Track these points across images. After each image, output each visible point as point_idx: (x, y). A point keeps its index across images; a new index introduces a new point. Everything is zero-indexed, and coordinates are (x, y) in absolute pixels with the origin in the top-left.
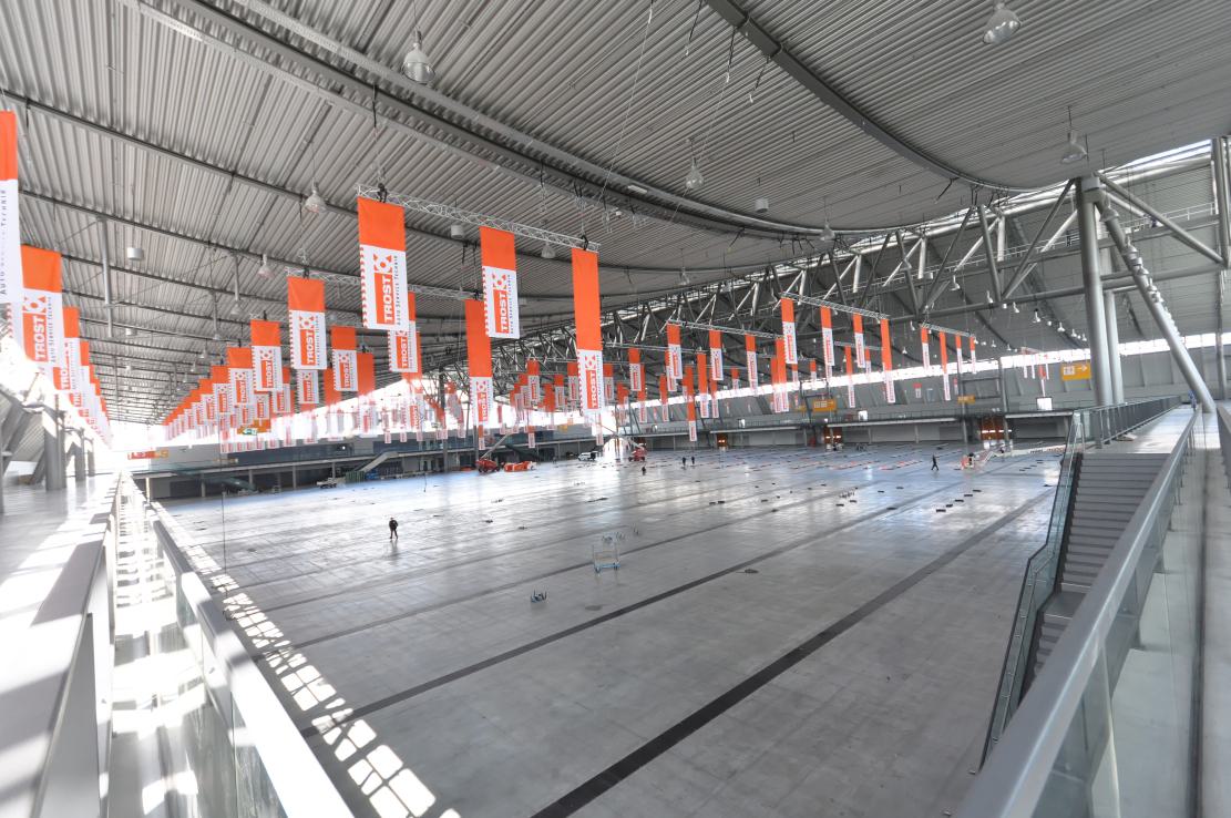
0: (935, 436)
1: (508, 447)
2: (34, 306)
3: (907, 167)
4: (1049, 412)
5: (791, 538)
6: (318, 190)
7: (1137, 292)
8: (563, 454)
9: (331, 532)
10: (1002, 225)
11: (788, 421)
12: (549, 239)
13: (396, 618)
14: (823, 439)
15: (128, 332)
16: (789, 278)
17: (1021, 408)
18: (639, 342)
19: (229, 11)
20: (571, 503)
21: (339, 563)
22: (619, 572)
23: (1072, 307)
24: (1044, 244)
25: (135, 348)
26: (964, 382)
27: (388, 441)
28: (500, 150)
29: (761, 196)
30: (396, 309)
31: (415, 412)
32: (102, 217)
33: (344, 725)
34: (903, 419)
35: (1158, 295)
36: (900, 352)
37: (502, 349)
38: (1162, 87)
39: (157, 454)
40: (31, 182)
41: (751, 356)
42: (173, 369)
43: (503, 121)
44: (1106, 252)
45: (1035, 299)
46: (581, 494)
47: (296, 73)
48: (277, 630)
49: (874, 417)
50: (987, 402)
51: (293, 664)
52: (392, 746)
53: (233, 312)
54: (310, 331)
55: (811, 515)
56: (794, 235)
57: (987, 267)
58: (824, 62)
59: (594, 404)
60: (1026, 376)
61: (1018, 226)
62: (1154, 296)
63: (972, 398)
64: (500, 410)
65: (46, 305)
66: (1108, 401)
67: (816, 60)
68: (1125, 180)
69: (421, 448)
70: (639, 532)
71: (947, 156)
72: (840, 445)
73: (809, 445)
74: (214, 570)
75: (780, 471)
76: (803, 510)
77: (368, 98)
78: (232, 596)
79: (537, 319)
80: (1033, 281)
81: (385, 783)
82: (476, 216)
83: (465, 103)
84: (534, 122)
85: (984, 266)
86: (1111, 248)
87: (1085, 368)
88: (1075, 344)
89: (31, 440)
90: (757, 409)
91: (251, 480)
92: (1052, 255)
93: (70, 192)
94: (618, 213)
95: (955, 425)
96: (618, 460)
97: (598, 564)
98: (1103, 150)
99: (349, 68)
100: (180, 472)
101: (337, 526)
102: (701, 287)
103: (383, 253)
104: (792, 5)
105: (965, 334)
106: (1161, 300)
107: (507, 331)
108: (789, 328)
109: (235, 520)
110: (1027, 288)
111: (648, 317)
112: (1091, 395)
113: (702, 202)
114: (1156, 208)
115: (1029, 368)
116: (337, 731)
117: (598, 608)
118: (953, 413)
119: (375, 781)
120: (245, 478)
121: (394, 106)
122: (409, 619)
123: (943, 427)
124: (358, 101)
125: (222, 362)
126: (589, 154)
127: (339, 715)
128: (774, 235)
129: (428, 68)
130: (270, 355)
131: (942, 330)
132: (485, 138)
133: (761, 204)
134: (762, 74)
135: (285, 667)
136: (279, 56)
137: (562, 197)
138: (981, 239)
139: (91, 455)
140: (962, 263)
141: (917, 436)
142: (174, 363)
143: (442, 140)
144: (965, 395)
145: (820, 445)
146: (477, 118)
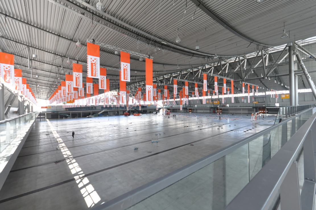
0: (247, 112)
1: (135, 109)
2: (7, 68)
3: (238, 39)
4: (278, 107)
5: (207, 136)
6: (79, 41)
7: (304, 75)
8: (149, 112)
9: (88, 129)
10: (268, 56)
11: (208, 106)
12: (141, 56)
13: (100, 152)
14: (217, 111)
15: (37, 76)
16: (209, 68)
17: (271, 106)
18: (169, 84)
19: (73, 2)
20: (151, 125)
21: (88, 137)
22: (158, 143)
23: (286, 79)
24: (279, 61)
25: (41, 81)
26: (255, 98)
27: (104, 107)
28: (127, 31)
29: (197, 45)
30: (96, 72)
31: (107, 100)
32: (28, 46)
33: (82, 178)
34: (238, 107)
35: (310, 76)
36: (238, 89)
37: (134, 84)
38: (312, 17)
39: (48, 107)
40: (10, 37)
41: (196, 89)
42: (50, 86)
43: (127, 23)
44: (296, 64)
45: (275, 76)
46: (152, 123)
47: (75, 10)
48: (70, 153)
49: (230, 106)
50: (262, 103)
51: (72, 162)
52: (92, 185)
53: (62, 72)
54: (78, 78)
55: (212, 131)
56: (208, 57)
57: (262, 67)
58: (214, 8)
59: (150, 100)
60: (272, 97)
61: (272, 56)
62: (308, 77)
63: (257, 102)
64: (133, 100)
65: (10, 68)
66: (293, 105)
67: (211, 8)
68: (303, 44)
69: (124, 108)
70: (168, 132)
71: (250, 36)
72: (221, 113)
73: (213, 113)
74: (58, 137)
75: (204, 119)
76: (210, 129)
77: (91, 16)
78: (61, 144)
79: (141, 77)
80: (276, 71)
81: (89, 194)
82: (124, 50)
83: (124, 22)
84: (135, 23)
85: (262, 67)
86: (298, 63)
87: (288, 95)
88: (286, 89)
89: (16, 102)
90: (200, 103)
91: (71, 115)
92: (281, 64)
93: (20, 40)
94: (159, 49)
95: (252, 109)
96: (163, 114)
97: (153, 141)
98: (295, 35)
99: (85, 7)
100: (53, 112)
101: (90, 128)
102: (186, 70)
103: (93, 57)
104: (217, 1)
105: (255, 85)
106: (310, 78)
107: (127, 80)
108: (205, 82)
109: (65, 125)
110: (274, 73)
111: (172, 78)
112: (289, 103)
113: (182, 47)
114: (311, 52)
115: (273, 95)
116: (80, 180)
117: (151, 152)
118: (252, 106)
119: (87, 193)
120: (69, 114)
121: (98, 18)
122: (103, 152)
123: (249, 110)
124: (89, 17)
125: (61, 85)
126: (159, 37)
127: (81, 176)
128: (203, 56)
129: (103, 7)
130: (70, 83)
131: (249, 84)
132: (123, 28)
133: (197, 48)
134: (195, 12)
135: (70, 163)
136: (67, 4)
137: (144, 44)
138: (262, 60)
139: (32, 107)
140: (256, 66)
141: (242, 112)
142: (51, 85)
143: (111, 28)
144: (255, 101)
145: (216, 113)
146: (120, 22)
